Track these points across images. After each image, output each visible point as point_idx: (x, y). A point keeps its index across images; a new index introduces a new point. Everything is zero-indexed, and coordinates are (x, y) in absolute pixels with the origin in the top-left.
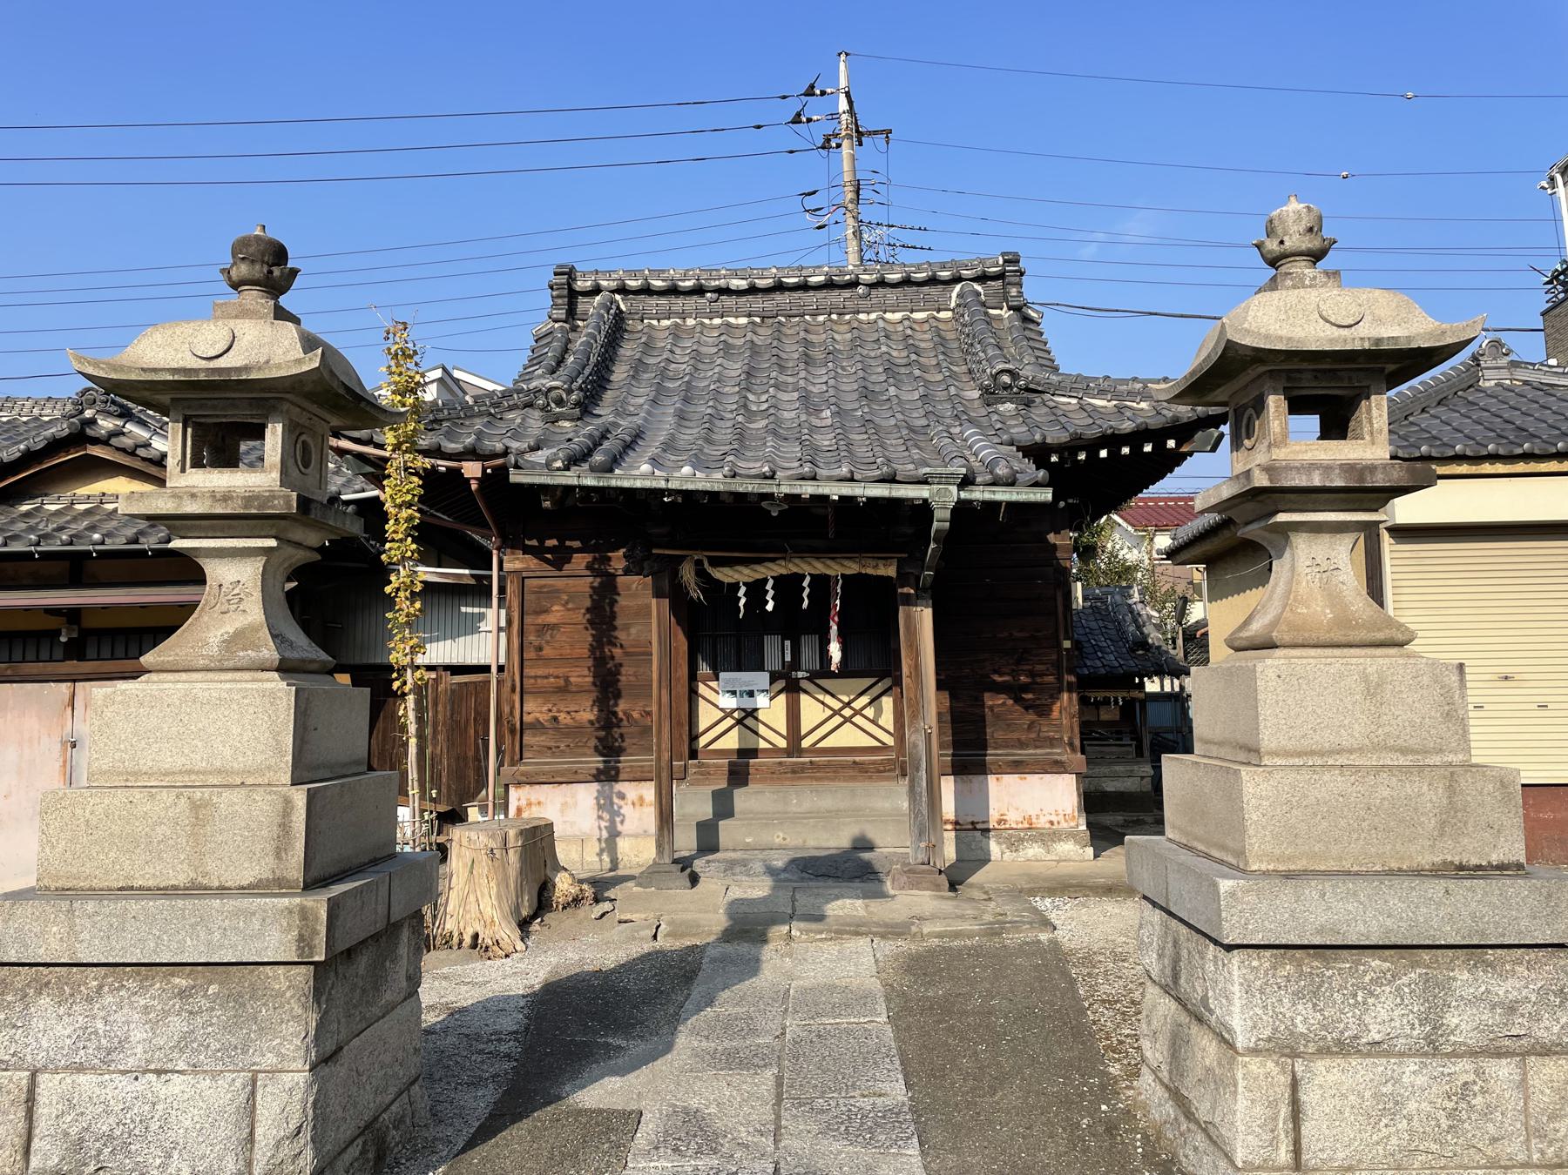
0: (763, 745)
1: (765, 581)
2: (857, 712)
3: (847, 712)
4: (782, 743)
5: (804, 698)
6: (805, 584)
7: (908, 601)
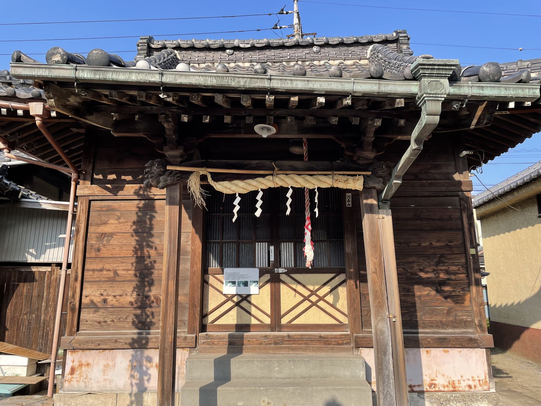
0: (254, 321)
1: (257, 192)
2: (321, 299)
3: (314, 298)
4: (267, 321)
5: (283, 287)
6: (289, 195)
7: (371, 209)
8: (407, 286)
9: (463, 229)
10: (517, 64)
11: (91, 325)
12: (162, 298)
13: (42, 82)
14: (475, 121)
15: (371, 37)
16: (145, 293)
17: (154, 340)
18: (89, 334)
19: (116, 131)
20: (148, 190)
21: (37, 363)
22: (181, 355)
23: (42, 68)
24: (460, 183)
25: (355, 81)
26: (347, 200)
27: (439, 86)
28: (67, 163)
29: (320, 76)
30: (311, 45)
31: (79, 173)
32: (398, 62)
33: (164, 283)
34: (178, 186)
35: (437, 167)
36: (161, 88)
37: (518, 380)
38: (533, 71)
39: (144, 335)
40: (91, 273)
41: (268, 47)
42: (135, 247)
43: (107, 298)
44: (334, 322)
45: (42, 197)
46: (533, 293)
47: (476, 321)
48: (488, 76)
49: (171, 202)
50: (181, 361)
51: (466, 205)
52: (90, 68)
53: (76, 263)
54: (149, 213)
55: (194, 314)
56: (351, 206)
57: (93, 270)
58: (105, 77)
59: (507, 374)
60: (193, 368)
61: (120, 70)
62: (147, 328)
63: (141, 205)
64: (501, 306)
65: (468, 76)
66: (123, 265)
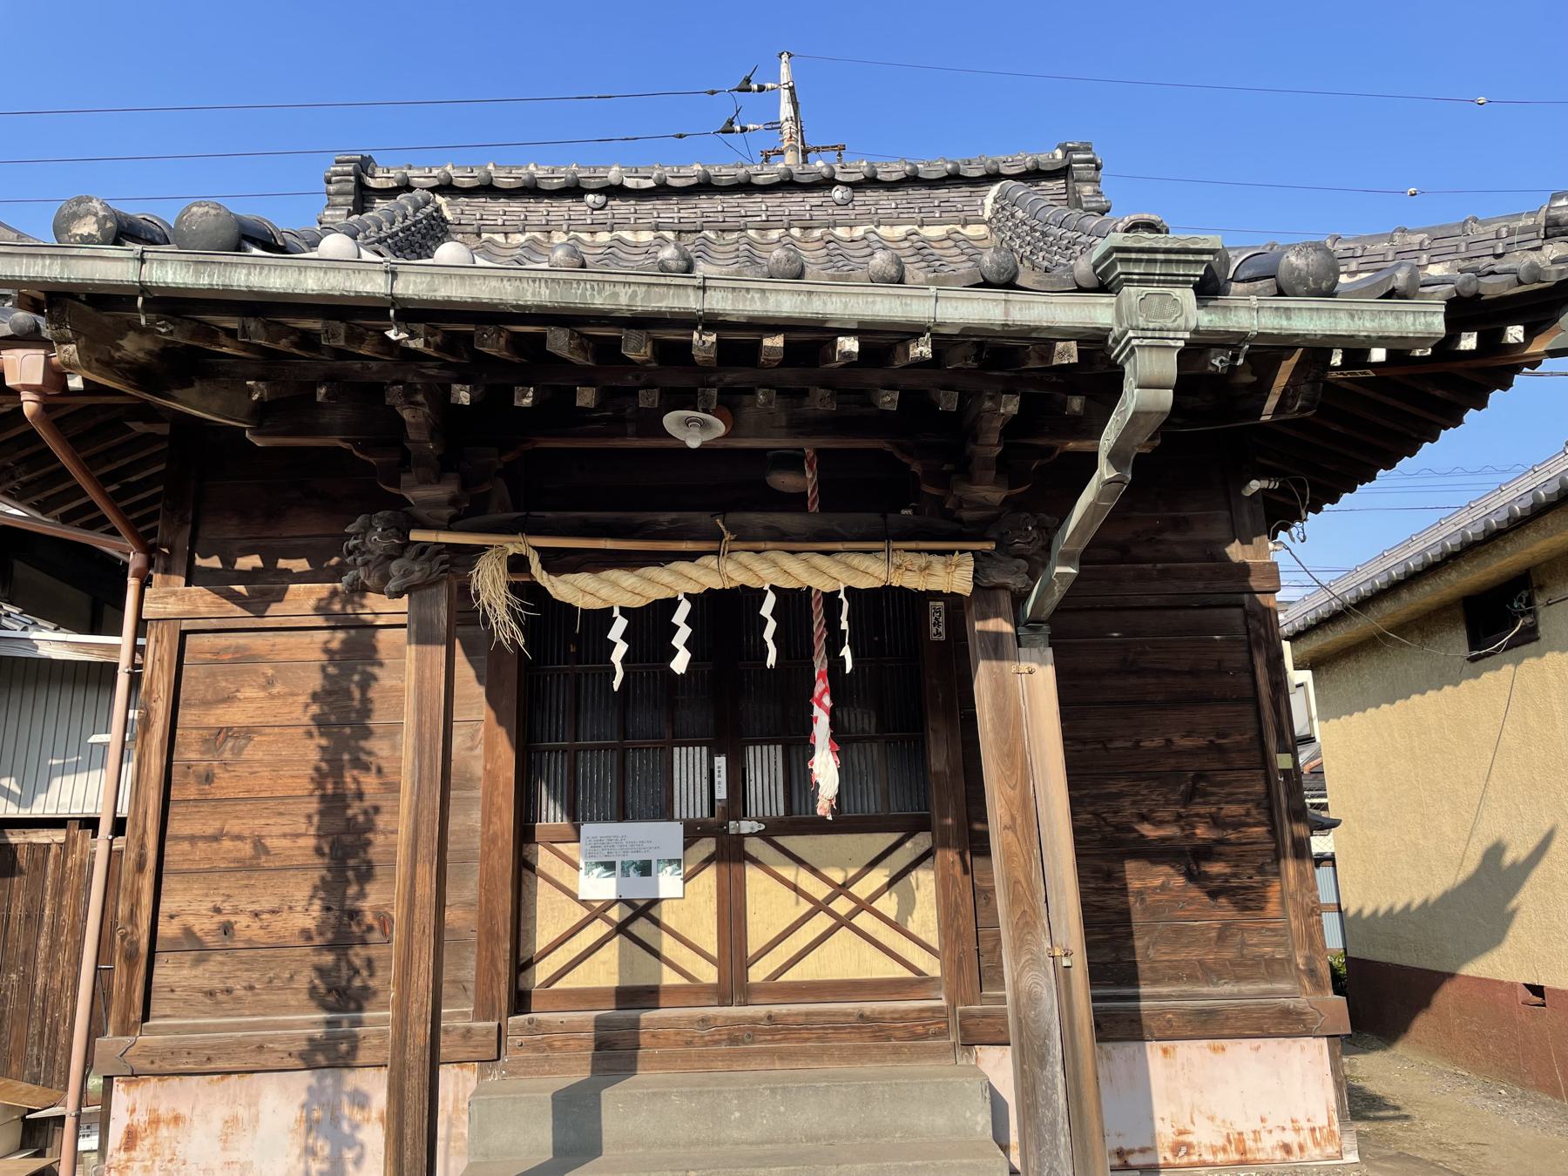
0: (670, 978)
1: (672, 604)
2: (863, 906)
3: (842, 906)
4: (708, 974)
5: (752, 874)
7: (996, 648)
8: (1105, 865)
9: (1255, 699)
10: (1391, 240)
11: (185, 1001)
12: (397, 914)
13: (42, 296)
14: (1272, 403)
15: (994, 162)
16: (348, 902)
17: (376, 1042)
18: (176, 1029)
19: (257, 432)
20: (356, 599)
21: (23, 1118)
22: (456, 1084)
23: (43, 256)
24: (1244, 569)
25: (941, 294)
26: (932, 620)
27: (1169, 308)
28: (115, 522)
29: (842, 279)
30: (828, 183)
31: (150, 551)
32: (1069, 234)
33: (401, 870)
34: (443, 590)
35: (1180, 524)
36: (392, 312)
37: (1428, 1126)
38: (1435, 259)
39: (345, 1028)
40: (186, 846)
41: (706, 187)
42: (317, 769)
43: (233, 919)
44: (902, 972)
45: (41, 622)
46: (1462, 877)
47: (1300, 961)
48: (1303, 280)
49: (422, 635)
50: (456, 1100)
51: (1262, 631)
52: (184, 257)
53: (140, 817)
54: (360, 668)
55: (493, 962)
56: (943, 638)
57: (192, 839)
58: (227, 282)
59: (1397, 1108)
60: (489, 1119)
61: (272, 261)
62: (352, 1005)
63: (335, 645)
64: (1375, 913)
65: (1249, 280)
66: (280, 820)
